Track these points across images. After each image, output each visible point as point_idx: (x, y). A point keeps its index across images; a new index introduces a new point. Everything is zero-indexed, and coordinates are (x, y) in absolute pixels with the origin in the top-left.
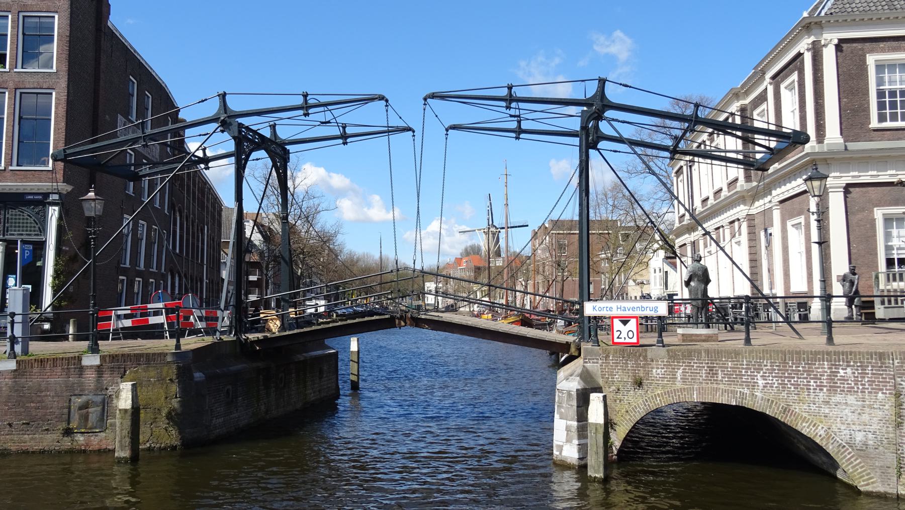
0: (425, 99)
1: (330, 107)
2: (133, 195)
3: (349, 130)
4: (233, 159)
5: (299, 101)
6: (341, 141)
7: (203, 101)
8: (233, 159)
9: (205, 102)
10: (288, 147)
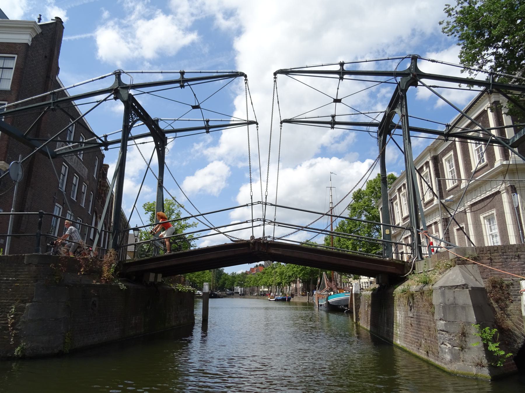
0: (275, 74)
1: (190, 83)
2: (76, 201)
3: (210, 124)
4: (119, 145)
5: (178, 77)
6: (205, 131)
8: (119, 145)
10: (167, 135)
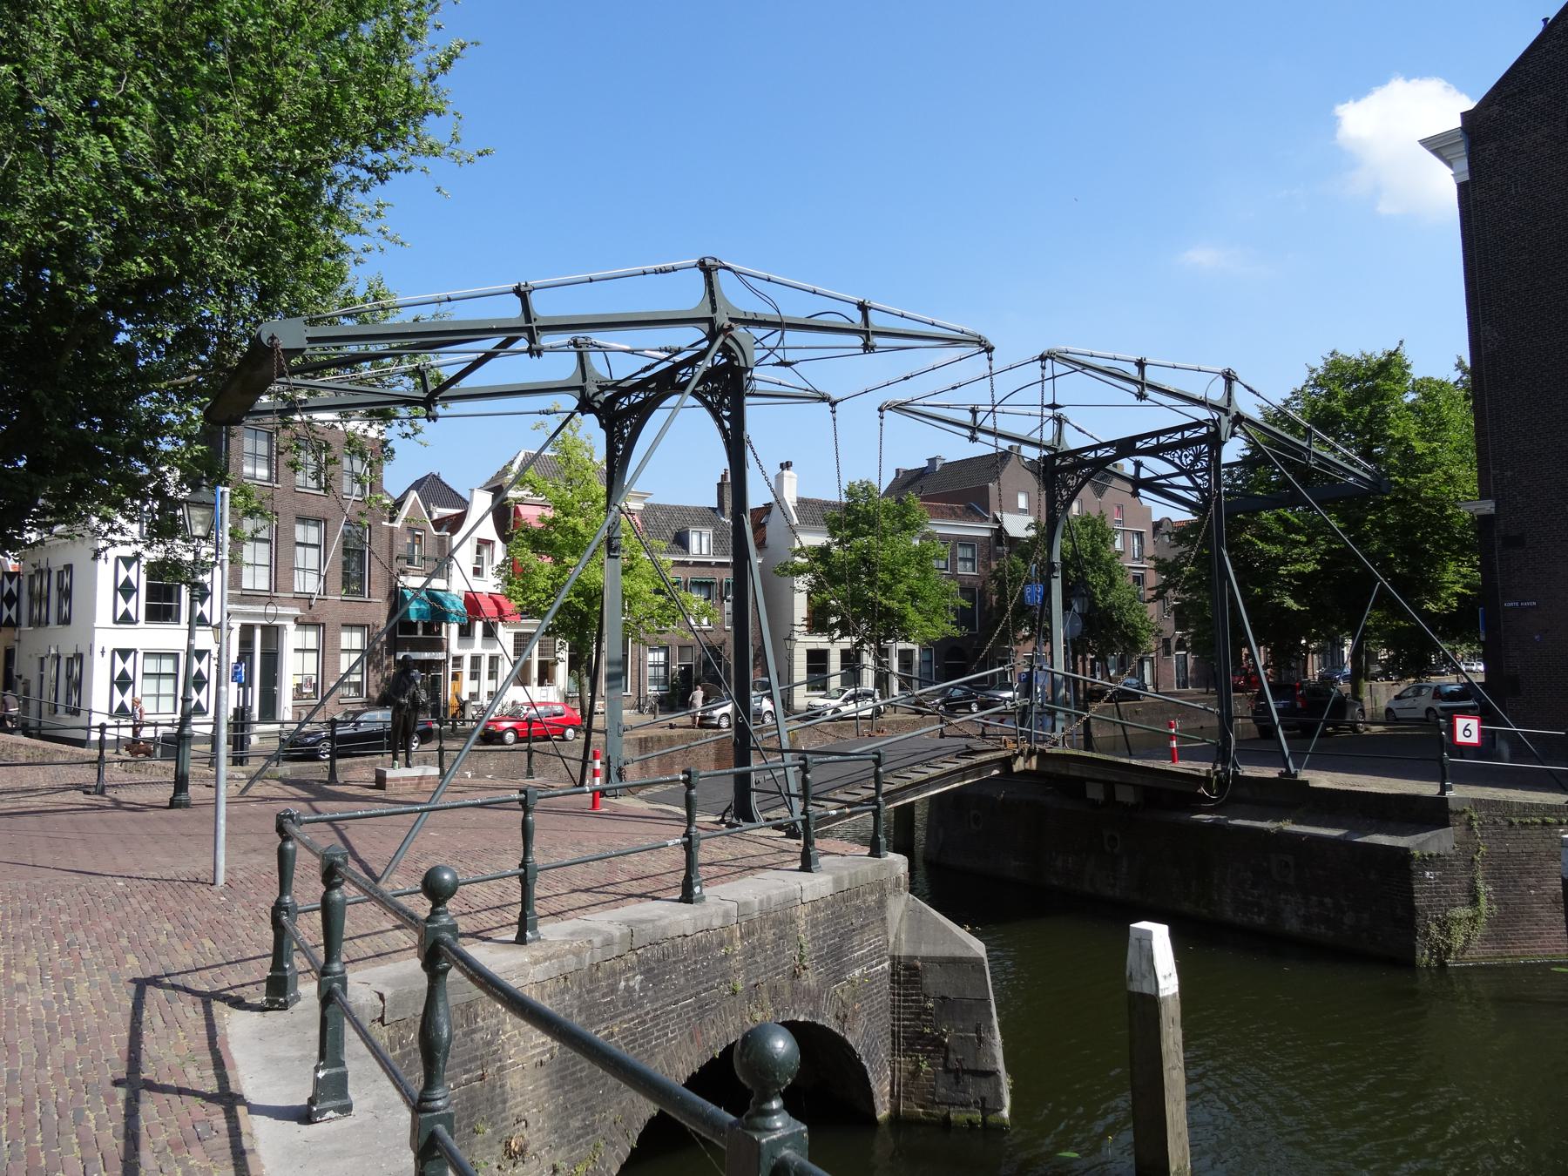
0: (1043, 358)
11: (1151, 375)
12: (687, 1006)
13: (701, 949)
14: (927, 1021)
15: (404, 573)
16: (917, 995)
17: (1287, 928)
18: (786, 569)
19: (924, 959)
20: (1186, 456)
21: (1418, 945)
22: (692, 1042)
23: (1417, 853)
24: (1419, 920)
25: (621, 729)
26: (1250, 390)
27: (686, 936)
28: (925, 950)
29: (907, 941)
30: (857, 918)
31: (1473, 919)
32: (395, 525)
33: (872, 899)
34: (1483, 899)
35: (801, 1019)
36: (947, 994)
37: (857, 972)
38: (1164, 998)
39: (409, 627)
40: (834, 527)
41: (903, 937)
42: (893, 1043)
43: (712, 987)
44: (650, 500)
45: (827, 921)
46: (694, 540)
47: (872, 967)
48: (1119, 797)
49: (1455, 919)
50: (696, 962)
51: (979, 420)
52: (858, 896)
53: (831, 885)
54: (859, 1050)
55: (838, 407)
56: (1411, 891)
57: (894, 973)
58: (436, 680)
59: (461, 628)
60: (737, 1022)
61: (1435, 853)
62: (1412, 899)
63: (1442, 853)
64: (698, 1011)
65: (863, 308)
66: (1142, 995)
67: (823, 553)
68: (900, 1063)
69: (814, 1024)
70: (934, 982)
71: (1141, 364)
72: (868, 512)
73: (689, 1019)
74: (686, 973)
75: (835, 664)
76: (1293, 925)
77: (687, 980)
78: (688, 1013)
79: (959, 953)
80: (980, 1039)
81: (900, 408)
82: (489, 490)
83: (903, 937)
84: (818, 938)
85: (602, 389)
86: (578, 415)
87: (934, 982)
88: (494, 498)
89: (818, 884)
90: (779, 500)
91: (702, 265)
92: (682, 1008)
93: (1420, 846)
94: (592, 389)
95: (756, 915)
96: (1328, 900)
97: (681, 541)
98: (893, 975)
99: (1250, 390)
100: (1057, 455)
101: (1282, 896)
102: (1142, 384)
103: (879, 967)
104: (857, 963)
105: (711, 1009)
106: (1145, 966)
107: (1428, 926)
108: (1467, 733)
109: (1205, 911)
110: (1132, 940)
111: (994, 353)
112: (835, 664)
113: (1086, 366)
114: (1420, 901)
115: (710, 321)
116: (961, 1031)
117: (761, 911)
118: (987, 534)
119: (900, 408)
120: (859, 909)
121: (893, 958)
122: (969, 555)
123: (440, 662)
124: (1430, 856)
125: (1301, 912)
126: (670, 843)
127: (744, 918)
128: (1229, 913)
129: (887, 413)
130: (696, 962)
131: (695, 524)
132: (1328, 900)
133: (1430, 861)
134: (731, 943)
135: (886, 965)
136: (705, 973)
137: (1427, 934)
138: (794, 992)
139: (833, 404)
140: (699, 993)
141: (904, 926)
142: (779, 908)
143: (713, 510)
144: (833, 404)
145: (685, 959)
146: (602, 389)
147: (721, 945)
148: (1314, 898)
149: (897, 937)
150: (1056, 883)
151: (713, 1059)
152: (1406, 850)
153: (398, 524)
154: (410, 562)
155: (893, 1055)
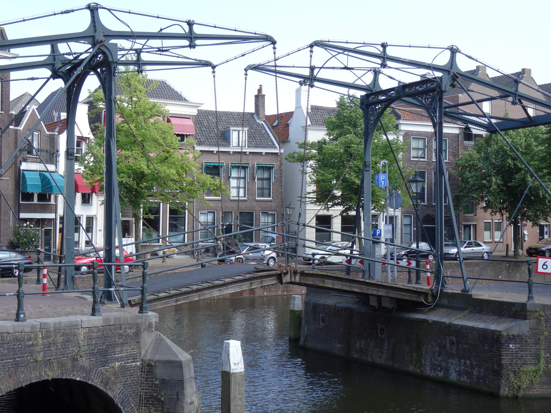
0: (311, 46)
7: (67, 12)
9: (64, 9)
11: (390, 52)
12: (8, 362)
13: (17, 339)
14: (155, 390)
15: (25, 160)
16: (152, 378)
17: (451, 379)
18: (293, 158)
19: (157, 361)
20: (428, 99)
21: (502, 385)
22: (10, 377)
23: (505, 334)
24: (504, 371)
25: (73, 255)
26: (470, 57)
27: (9, 333)
28: (157, 357)
29: (151, 353)
30: (119, 338)
31: (536, 372)
32: (19, 128)
33: (131, 332)
34: (542, 361)
35: (78, 379)
36: (165, 378)
37: (117, 364)
38: (234, 373)
39: (28, 197)
40: (331, 127)
41: (150, 351)
42: (140, 400)
43: (23, 357)
44: (202, 108)
45: (98, 338)
46: (234, 136)
47: (128, 363)
48: (384, 305)
49: (524, 372)
50: (14, 345)
51: (315, 74)
52: (121, 328)
53: (101, 321)
54: (116, 400)
55: (216, 70)
56: (500, 355)
57: (142, 368)
58: (47, 233)
59: (84, 196)
60: (37, 374)
61: (516, 334)
62: (500, 359)
63: (520, 334)
64: (14, 366)
65: (190, 24)
66: (225, 372)
67: (320, 145)
68: (142, 409)
69: (86, 383)
70: (160, 372)
71: (384, 46)
72: (351, 116)
73: (9, 368)
74: (8, 349)
75: (337, 224)
76: (453, 377)
77: (9, 352)
78: (8, 365)
79: (172, 358)
80: (178, 399)
81: (256, 68)
82: (87, 103)
83: (150, 351)
84: (91, 345)
85: (64, 64)
86: (52, 79)
87: (160, 372)
88: (90, 109)
89: (97, 320)
90: (298, 107)
91: (89, 7)
92: (5, 363)
93: (507, 330)
94: (58, 65)
95: (52, 329)
96: (468, 362)
97: (225, 138)
98: (142, 368)
99: (470, 57)
100: (372, 94)
101: (450, 360)
102: (383, 58)
103: (134, 364)
104: (117, 360)
105: (22, 366)
106: (226, 359)
107: (509, 375)
108: (545, 267)
109: (418, 370)
110: (225, 345)
111: (276, 46)
112: (337, 224)
113: (345, 49)
114: (505, 361)
115: (93, 37)
116: (170, 395)
117: (55, 328)
118: (457, 131)
119: (256, 68)
120: (121, 335)
121: (142, 360)
122: (421, 146)
123: (50, 220)
124: (513, 336)
125: (457, 369)
126: (7, 294)
127: (44, 330)
128: (428, 372)
129: (250, 72)
130: (14, 345)
131: (236, 125)
132: (468, 362)
133: (513, 339)
134: (36, 339)
135: (138, 364)
136: (19, 351)
137: (508, 379)
138: (74, 366)
139: (214, 67)
140: (16, 358)
141: (152, 346)
142: (67, 328)
143: (252, 114)
144: (214, 67)
145: (8, 343)
146: (64, 64)
147: (30, 339)
148: (463, 361)
149: (147, 351)
150: (356, 356)
151: (22, 387)
152: (500, 332)
153: (21, 128)
154: (30, 152)
155: (140, 406)
